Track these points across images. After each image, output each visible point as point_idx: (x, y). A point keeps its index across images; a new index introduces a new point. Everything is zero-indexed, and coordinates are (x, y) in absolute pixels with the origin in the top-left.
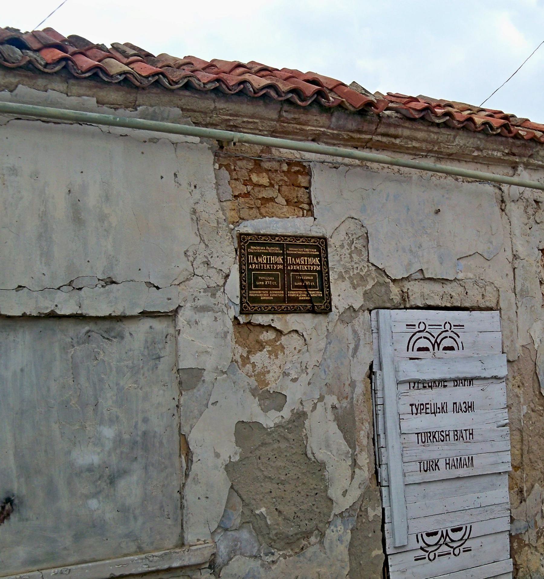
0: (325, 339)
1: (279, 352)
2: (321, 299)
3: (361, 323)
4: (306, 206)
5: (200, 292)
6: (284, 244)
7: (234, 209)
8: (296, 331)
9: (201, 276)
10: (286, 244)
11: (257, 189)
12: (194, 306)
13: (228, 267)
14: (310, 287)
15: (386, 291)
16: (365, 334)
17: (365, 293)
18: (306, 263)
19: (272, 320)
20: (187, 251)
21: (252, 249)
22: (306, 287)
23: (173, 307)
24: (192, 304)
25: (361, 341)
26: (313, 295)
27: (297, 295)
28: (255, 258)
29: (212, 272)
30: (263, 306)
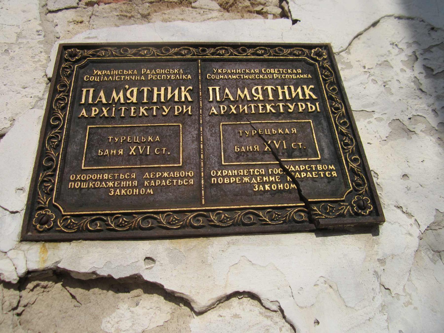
6: (196, 60)
7: (81, 22)
8: (253, 296)
13: (9, 115)
14: (290, 153)
18: (271, 98)
21: (97, 75)
27: (246, 179)
28: (102, 94)
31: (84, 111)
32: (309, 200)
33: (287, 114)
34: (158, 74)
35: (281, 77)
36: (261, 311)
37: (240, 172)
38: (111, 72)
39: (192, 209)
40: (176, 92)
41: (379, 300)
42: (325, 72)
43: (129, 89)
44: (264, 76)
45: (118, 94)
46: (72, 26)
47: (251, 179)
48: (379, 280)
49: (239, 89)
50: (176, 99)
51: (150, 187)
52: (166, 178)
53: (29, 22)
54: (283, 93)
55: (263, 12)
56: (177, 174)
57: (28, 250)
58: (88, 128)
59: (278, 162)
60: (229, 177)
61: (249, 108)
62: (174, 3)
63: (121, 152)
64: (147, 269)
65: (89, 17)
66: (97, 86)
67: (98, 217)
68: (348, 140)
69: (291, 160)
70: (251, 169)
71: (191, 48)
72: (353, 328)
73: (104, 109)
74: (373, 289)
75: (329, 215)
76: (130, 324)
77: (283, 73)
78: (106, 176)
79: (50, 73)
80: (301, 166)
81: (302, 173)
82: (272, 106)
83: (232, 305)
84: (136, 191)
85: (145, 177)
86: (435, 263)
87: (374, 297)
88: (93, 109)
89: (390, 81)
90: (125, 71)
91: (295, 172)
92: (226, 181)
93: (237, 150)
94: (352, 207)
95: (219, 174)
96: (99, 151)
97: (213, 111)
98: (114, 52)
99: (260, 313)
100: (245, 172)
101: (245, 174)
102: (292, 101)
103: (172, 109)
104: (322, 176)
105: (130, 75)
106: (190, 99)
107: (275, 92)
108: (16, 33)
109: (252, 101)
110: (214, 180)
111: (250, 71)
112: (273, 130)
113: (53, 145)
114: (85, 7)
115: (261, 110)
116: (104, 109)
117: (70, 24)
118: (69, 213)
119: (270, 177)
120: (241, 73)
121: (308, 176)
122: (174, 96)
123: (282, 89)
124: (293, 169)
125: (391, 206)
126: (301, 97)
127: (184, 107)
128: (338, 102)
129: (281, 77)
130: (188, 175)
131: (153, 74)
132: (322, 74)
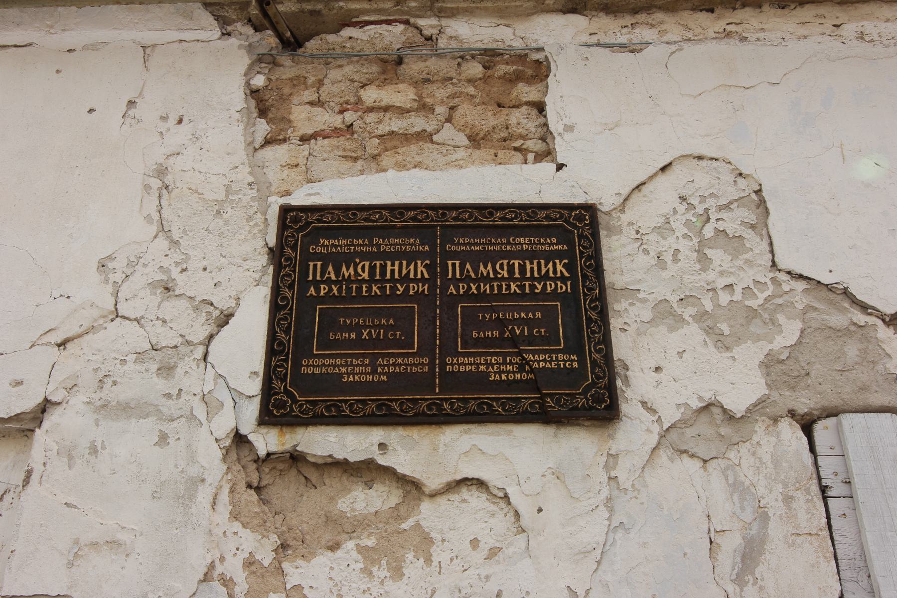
0: (604, 513)
1: (410, 556)
2: (572, 377)
3: (767, 458)
4: (539, 146)
5: (124, 362)
6: (435, 227)
7: (297, 165)
8: (480, 484)
9: (136, 320)
10: (441, 226)
11: (372, 117)
12: (98, 403)
13: (233, 294)
14: (531, 341)
15: (864, 352)
16: (788, 500)
17: (770, 363)
18: (517, 275)
19: (382, 446)
20: (110, 258)
21: (323, 245)
22: (514, 341)
23: (28, 403)
24: (93, 396)
25: (772, 525)
26: (542, 365)
27: (482, 368)
28: (330, 268)
29: (175, 308)
30: (346, 401)
31: (312, 289)
32: (544, 392)
33: (533, 295)
34: (391, 245)
35: (532, 248)
36: (489, 497)
37: (477, 360)
38: (339, 242)
39: (426, 397)
40: (412, 267)
41: (605, 492)
42: (584, 243)
43: (360, 263)
44: (511, 248)
45: (348, 269)
46: (286, 171)
47: (487, 368)
48: (608, 474)
49: (481, 264)
50: (412, 276)
51: (383, 373)
52: (400, 365)
53: (236, 170)
54: (532, 269)
55: (522, 149)
56: (411, 360)
57: (267, 433)
58: (318, 309)
59: (517, 350)
60: (465, 365)
61: (492, 287)
62: (410, 136)
63: (353, 336)
64: (381, 454)
65: (305, 159)
66: (326, 259)
67: (332, 403)
68: (597, 328)
69: (530, 348)
70: (489, 356)
71: (429, 212)
72: (574, 517)
73: (333, 286)
74: (600, 482)
75: (563, 407)
76: (364, 505)
77: (535, 243)
78: (339, 361)
79: (272, 241)
80: (541, 356)
81: (541, 363)
82: (517, 286)
83: (461, 491)
84: (370, 378)
85: (378, 363)
86: (672, 462)
87: (600, 490)
88: (322, 286)
89: (666, 251)
90: (355, 240)
91: (534, 362)
92: (461, 368)
93: (475, 335)
94: (588, 400)
95: (455, 361)
96: (331, 335)
97: (451, 290)
98: (342, 216)
99: (487, 499)
100: (482, 360)
101: (482, 362)
102: (539, 280)
103: (407, 289)
104: (562, 366)
105: (361, 245)
106: (426, 276)
107: (522, 268)
108: (224, 185)
109: (496, 279)
110: (449, 368)
111: (496, 241)
112: (515, 315)
113: (283, 327)
114: (299, 143)
115: (504, 290)
116: (333, 286)
117: (283, 169)
118: (303, 399)
119: (508, 366)
120: (486, 244)
121: (547, 366)
122: (409, 272)
123: (530, 264)
124: (532, 358)
125: (634, 401)
126: (551, 275)
127: (420, 285)
128: (592, 280)
129: (532, 248)
130: (423, 362)
131: (386, 245)
132: (579, 245)
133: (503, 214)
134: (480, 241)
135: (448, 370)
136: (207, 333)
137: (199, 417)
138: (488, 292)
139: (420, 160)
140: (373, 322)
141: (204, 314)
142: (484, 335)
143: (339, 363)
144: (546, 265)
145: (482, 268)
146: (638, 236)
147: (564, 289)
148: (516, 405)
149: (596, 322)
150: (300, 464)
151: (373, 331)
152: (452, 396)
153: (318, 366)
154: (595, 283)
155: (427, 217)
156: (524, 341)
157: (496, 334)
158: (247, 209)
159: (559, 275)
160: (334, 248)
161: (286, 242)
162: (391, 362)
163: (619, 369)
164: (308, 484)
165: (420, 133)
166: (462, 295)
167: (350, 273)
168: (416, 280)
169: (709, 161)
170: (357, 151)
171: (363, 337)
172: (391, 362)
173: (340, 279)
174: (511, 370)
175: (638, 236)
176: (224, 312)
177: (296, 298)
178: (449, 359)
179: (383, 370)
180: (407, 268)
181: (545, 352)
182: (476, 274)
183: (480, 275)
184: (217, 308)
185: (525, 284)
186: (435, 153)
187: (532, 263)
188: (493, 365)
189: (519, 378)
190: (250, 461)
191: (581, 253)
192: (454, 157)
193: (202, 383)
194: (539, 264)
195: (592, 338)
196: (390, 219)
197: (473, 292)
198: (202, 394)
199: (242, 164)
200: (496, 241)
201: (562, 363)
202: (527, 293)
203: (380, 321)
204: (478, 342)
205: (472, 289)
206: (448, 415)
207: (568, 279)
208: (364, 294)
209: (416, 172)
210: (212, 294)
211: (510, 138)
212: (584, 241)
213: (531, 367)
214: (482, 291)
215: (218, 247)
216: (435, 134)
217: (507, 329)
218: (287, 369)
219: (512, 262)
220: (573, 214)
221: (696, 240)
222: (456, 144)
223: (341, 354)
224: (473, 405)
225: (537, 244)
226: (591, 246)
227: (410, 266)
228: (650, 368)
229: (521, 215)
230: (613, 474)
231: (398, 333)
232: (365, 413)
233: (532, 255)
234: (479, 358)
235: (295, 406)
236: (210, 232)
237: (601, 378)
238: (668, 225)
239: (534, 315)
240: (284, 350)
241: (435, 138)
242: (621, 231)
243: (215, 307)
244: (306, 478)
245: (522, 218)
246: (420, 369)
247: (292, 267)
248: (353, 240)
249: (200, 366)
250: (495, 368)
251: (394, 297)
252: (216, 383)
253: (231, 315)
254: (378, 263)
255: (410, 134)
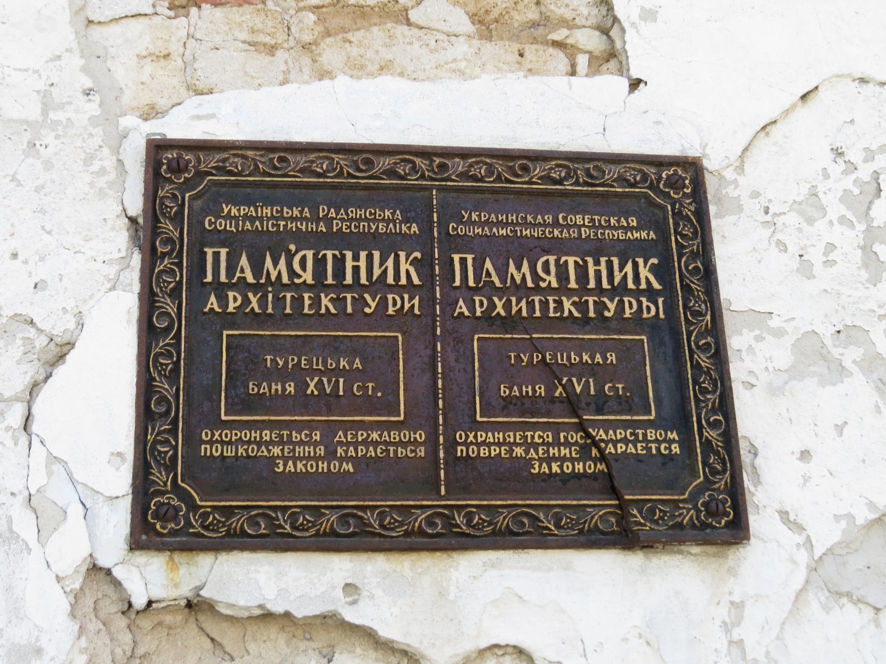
6: (429, 189)
7: (167, 56)
10: (440, 189)
14: (601, 404)
18: (573, 285)
19: (350, 588)
21: (229, 216)
22: (572, 405)
26: (621, 447)
27: (519, 451)
28: (244, 261)
30: (284, 509)
31: (213, 299)
34: (351, 220)
37: (509, 436)
38: (257, 212)
39: (425, 503)
40: (390, 263)
43: (296, 252)
44: (561, 232)
45: (275, 263)
46: (149, 68)
47: (527, 452)
50: (390, 280)
51: (348, 459)
52: (376, 444)
53: (58, 63)
57: (146, 565)
60: (489, 445)
61: (531, 305)
62: (369, 9)
63: (291, 388)
65: (182, 44)
68: (709, 384)
69: (601, 417)
70: (529, 431)
71: (418, 161)
73: (250, 295)
78: (267, 435)
79: (136, 205)
80: (618, 431)
81: (619, 445)
86: (827, 613)
88: (231, 294)
89: (813, 246)
90: (285, 210)
91: (606, 442)
92: (482, 452)
93: (505, 392)
94: (698, 511)
95: (471, 438)
96: (251, 386)
98: (260, 162)
100: (518, 437)
101: (518, 441)
104: (654, 452)
106: (416, 281)
108: (38, 92)
110: (462, 451)
111: (535, 218)
112: (573, 356)
115: (551, 310)
117: (143, 62)
119: (562, 448)
120: (518, 224)
121: (629, 451)
122: (385, 272)
124: (604, 437)
126: (631, 285)
127: (406, 296)
129: (596, 234)
130: (415, 438)
131: (342, 220)
132: (676, 233)
133: (545, 170)
134: (507, 219)
135: (459, 454)
136: (27, 380)
137: (23, 535)
138: (524, 313)
139: (390, 57)
140: (325, 363)
141: (19, 342)
142: (521, 391)
143: (268, 438)
144: (621, 269)
145: (512, 269)
146: (768, 218)
147: (653, 312)
148: (578, 519)
149: (708, 373)
150: (202, 618)
151: (325, 380)
152: (469, 502)
153: (230, 443)
154: (705, 302)
155: (414, 169)
156: (588, 404)
157: (541, 390)
158: (84, 140)
159: (643, 286)
160: (248, 223)
161: (161, 209)
162: (360, 439)
163: (745, 456)
164: (217, 652)
165: (386, 5)
166: (479, 318)
167: (279, 272)
168: (396, 288)
169: (877, 87)
170: (275, 33)
171: (309, 392)
172: (360, 439)
173: (263, 281)
174: (568, 455)
175: (768, 218)
176: (55, 339)
177: (186, 317)
178: (461, 435)
179: (346, 452)
180: (381, 265)
181: (626, 425)
182: (503, 281)
183: (509, 281)
184: (42, 331)
185: (587, 302)
186: (416, 45)
187: (597, 263)
188: (536, 446)
189: (581, 471)
190: (116, 613)
191: (680, 246)
192: (450, 54)
193: (25, 473)
194: (610, 264)
195: (702, 401)
196: (348, 172)
197: (498, 313)
198: (27, 494)
199: (67, 50)
200: (535, 221)
201: (653, 446)
202: (591, 318)
203: (338, 363)
204: (509, 405)
205: (496, 307)
206: (463, 534)
207: (658, 293)
208: (306, 311)
209: (386, 81)
210: (32, 304)
211: (542, 23)
212: (685, 226)
213: (601, 451)
214: (514, 312)
215: (36, 214)
216: (413, 7)
217: (560, 382)
218: (175, 448)
219: (563, 259)
220: (664, 175)
221: (861, 227)
222: (451, 30)
223: (270, 421)
224: (504, 519)
225: (604, 228)
226: (695, 233)
227: (386, 261)
228: (793, 453)
229: (575, 173)
230: (736, 636)
231: (370, 385)
232: (319, 529)
233: (598, 249)
234: (511, 434)
235: (194, 517)
236: (19, 184)
237: (718, 473)
238: (814, 198)
239: (605, 358)
240: (168, 412)
241: (413, 15)
242: (740, 208)
243: (38, 329)
244: (212, 640)
245: (578, 178)
246: (412, 451)
247: (176, 257)
248: (282, 210)
249: (20, 442)
250: (541, 452)
251: (360, 318)
252: (50, 474)
253: (71, 345)
254: (329, 254)
255: (368, 6)
